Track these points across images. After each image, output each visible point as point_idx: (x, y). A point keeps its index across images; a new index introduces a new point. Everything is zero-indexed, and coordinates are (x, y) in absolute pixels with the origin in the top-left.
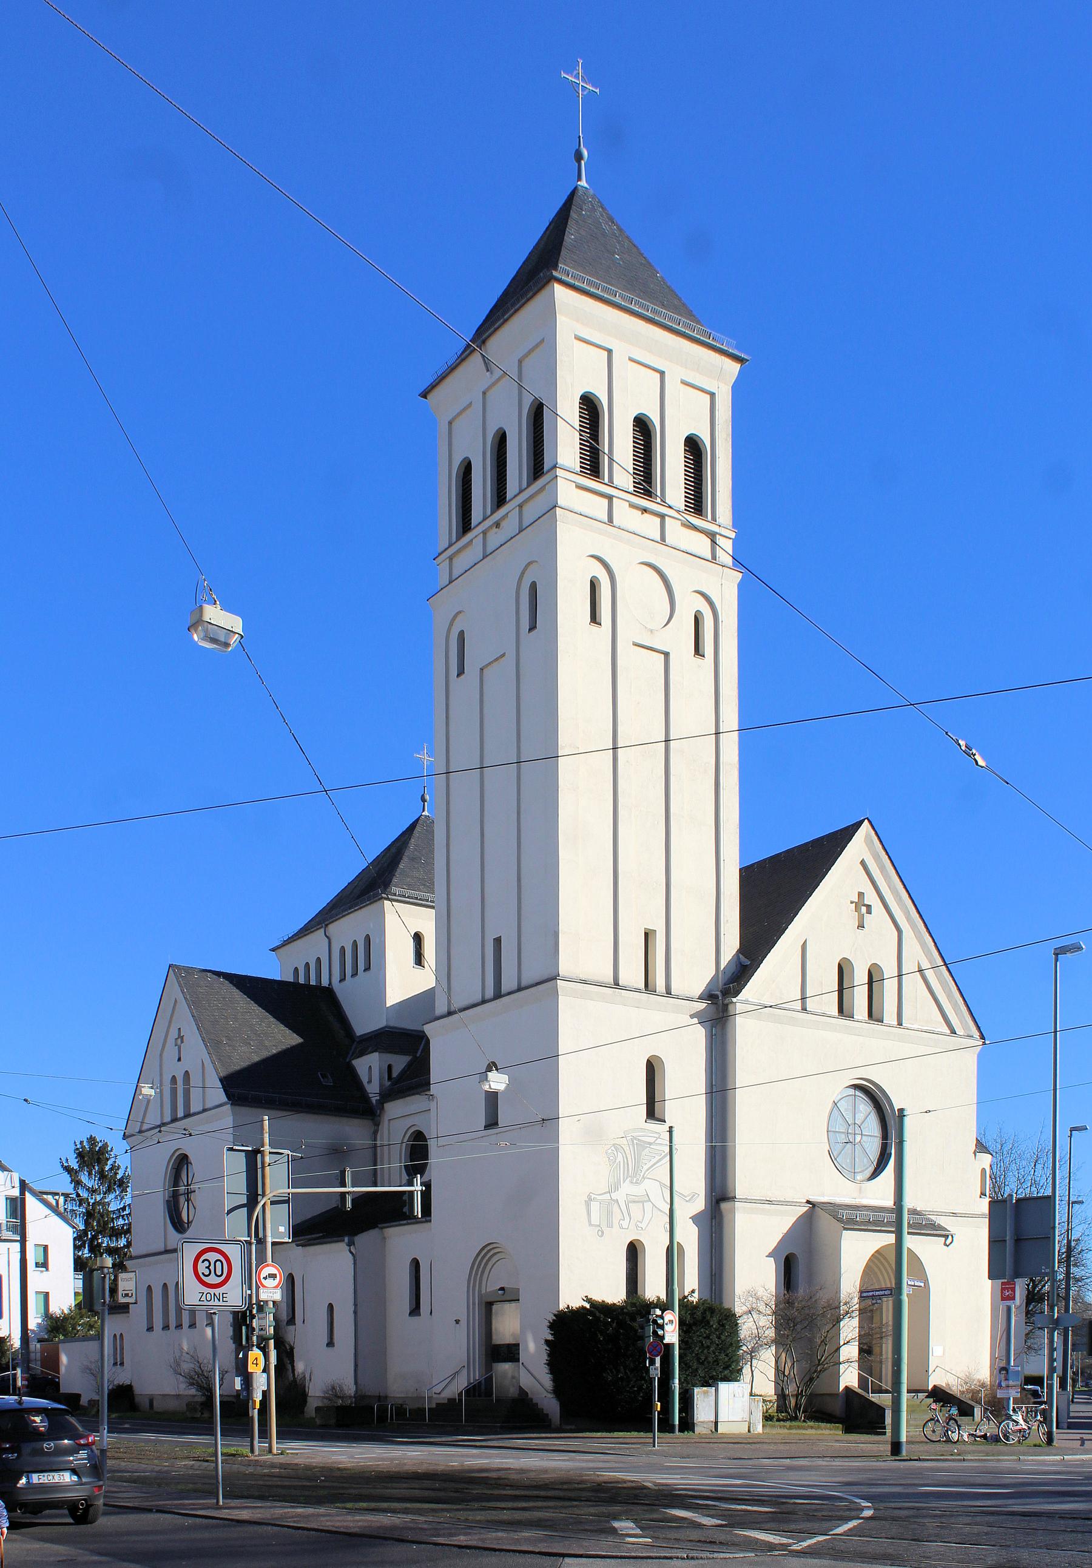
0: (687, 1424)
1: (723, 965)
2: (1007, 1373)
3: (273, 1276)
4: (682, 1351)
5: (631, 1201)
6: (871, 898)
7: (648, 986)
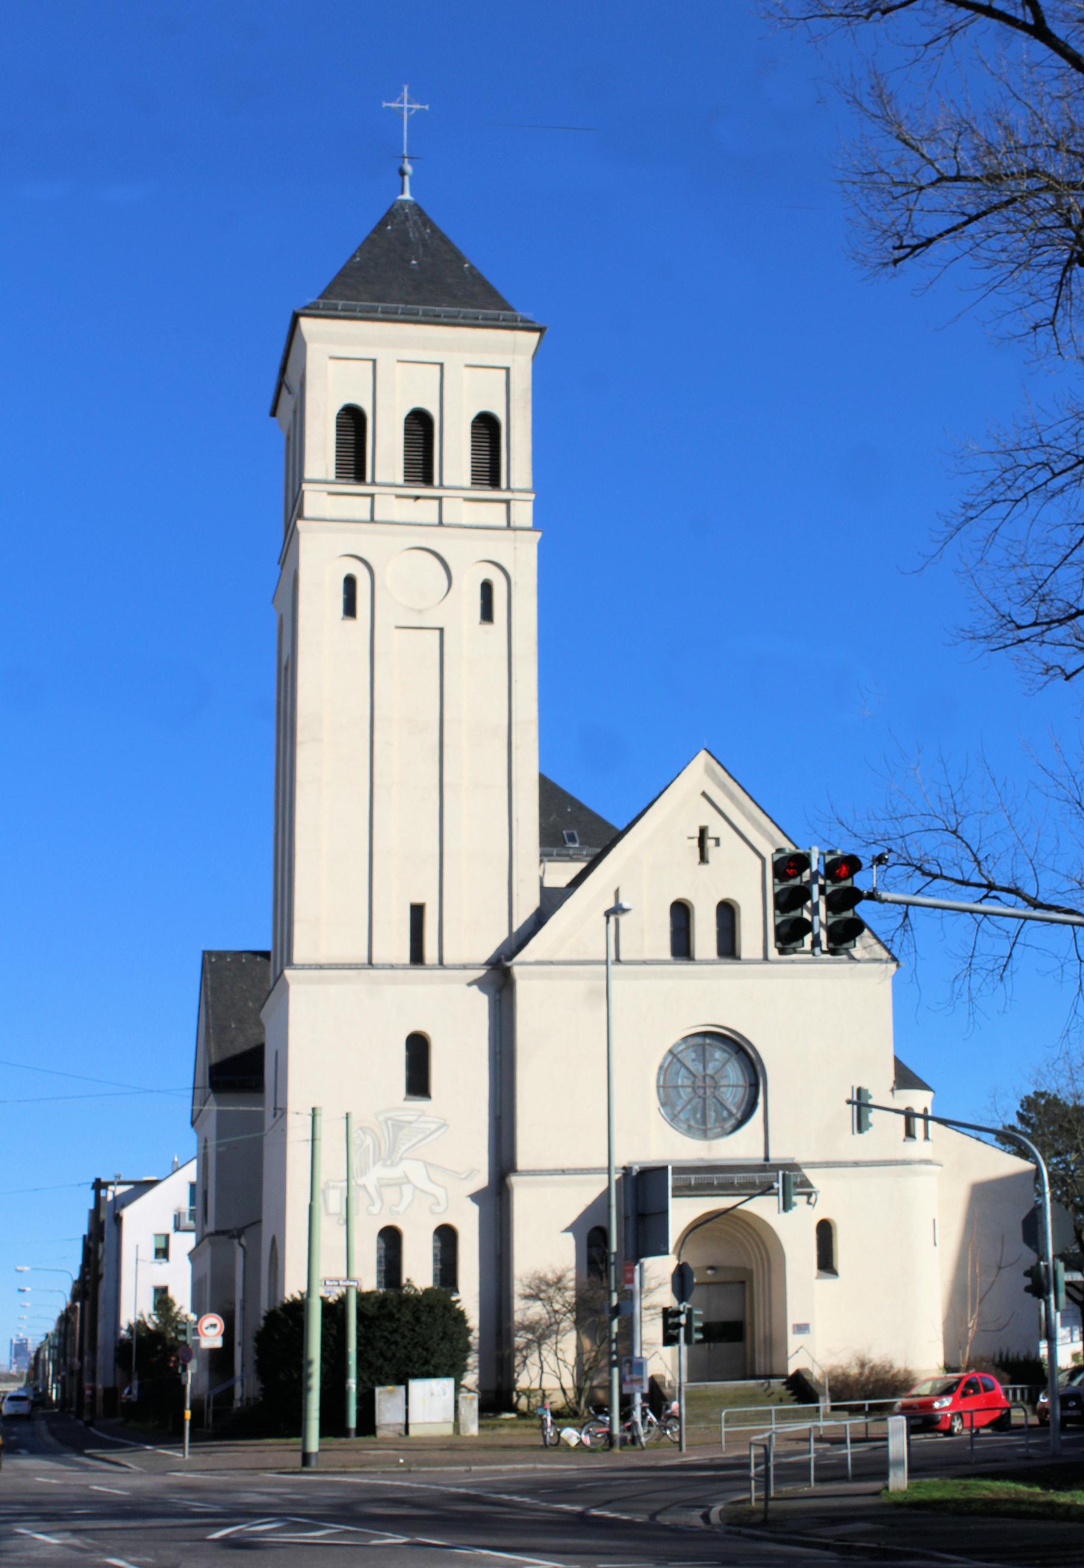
0: (368, 1424)
2: (631, 1366)
4: (362, 1348)
5: (383, 1185)
6: (717, 828)
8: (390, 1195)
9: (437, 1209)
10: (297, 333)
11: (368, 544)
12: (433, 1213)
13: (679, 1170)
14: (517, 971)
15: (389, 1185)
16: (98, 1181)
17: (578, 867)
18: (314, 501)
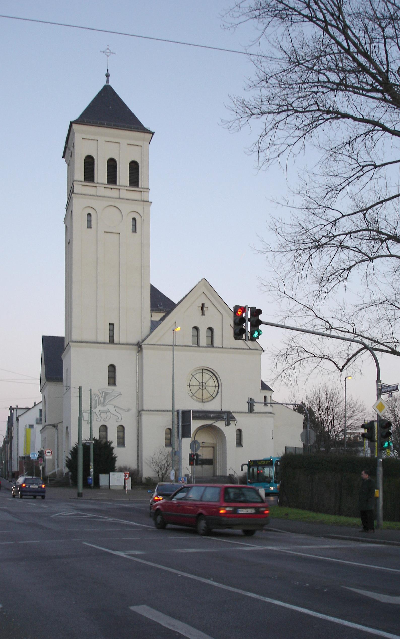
1: (215, 421)
3: (49, 452)
5: (101, 412)
7: (112, 341)
8: (104, 415)
9: (118, 420)
10: (72, 129)
11: (98, 204)
12: (117, 421)
13: (194, 412)
14: (143, 346)
15: (103, 412)
16: (11, 407)
17: (162, 315)
18: (78, 188)
